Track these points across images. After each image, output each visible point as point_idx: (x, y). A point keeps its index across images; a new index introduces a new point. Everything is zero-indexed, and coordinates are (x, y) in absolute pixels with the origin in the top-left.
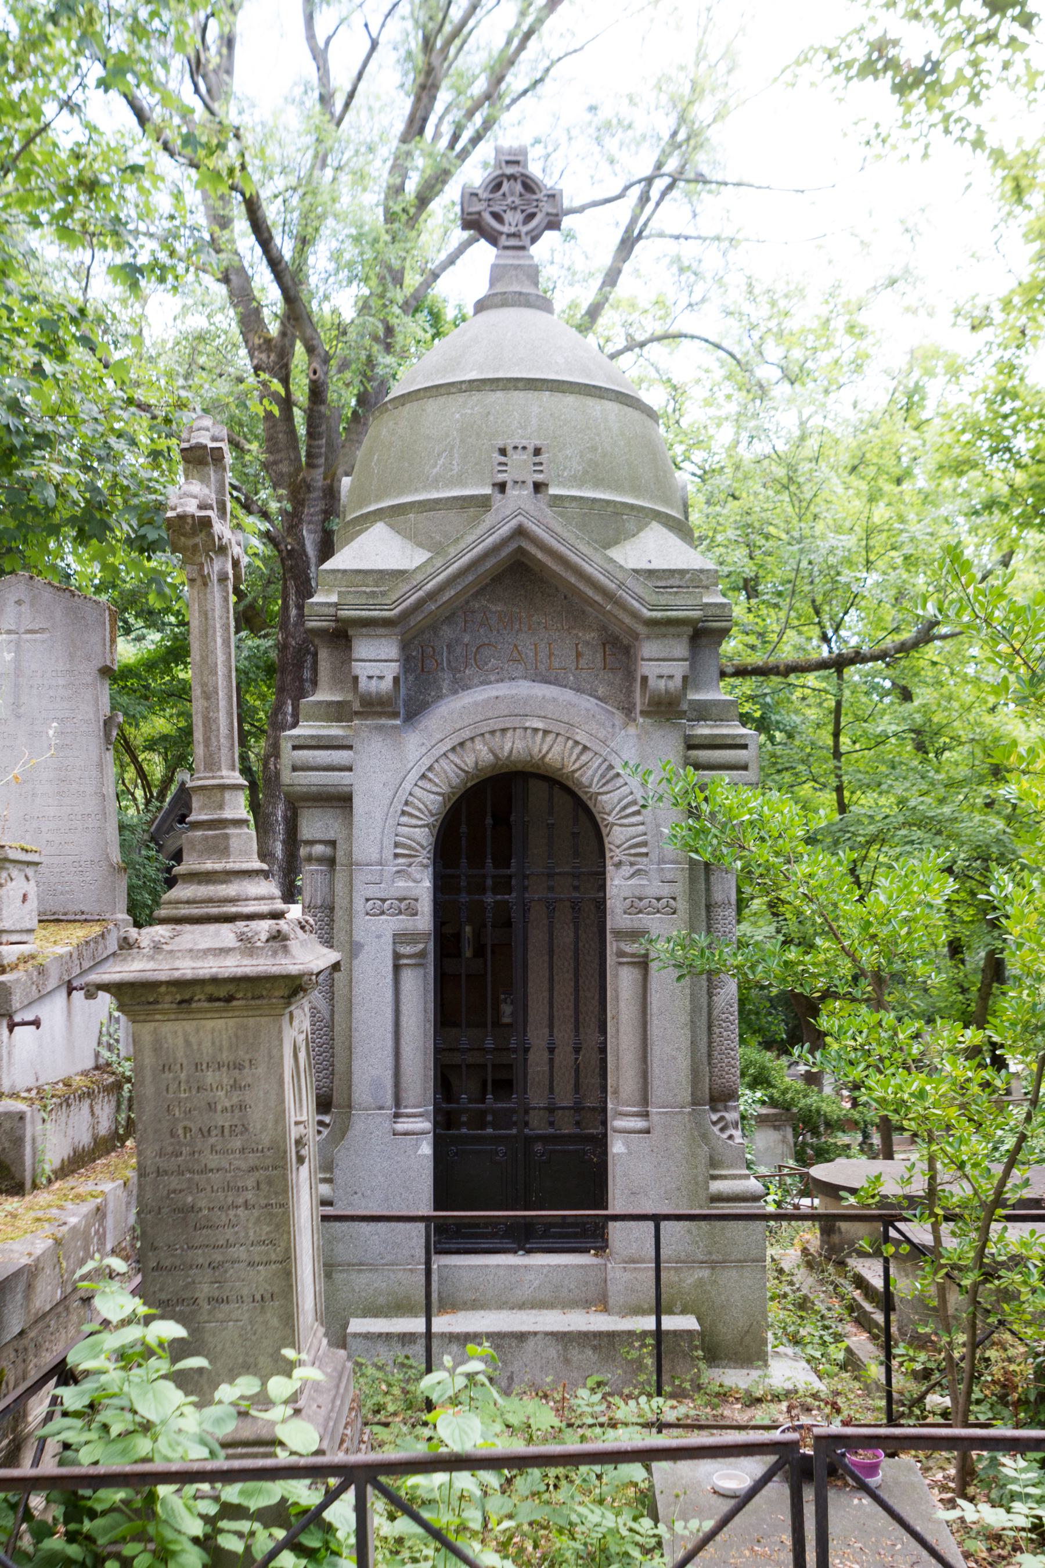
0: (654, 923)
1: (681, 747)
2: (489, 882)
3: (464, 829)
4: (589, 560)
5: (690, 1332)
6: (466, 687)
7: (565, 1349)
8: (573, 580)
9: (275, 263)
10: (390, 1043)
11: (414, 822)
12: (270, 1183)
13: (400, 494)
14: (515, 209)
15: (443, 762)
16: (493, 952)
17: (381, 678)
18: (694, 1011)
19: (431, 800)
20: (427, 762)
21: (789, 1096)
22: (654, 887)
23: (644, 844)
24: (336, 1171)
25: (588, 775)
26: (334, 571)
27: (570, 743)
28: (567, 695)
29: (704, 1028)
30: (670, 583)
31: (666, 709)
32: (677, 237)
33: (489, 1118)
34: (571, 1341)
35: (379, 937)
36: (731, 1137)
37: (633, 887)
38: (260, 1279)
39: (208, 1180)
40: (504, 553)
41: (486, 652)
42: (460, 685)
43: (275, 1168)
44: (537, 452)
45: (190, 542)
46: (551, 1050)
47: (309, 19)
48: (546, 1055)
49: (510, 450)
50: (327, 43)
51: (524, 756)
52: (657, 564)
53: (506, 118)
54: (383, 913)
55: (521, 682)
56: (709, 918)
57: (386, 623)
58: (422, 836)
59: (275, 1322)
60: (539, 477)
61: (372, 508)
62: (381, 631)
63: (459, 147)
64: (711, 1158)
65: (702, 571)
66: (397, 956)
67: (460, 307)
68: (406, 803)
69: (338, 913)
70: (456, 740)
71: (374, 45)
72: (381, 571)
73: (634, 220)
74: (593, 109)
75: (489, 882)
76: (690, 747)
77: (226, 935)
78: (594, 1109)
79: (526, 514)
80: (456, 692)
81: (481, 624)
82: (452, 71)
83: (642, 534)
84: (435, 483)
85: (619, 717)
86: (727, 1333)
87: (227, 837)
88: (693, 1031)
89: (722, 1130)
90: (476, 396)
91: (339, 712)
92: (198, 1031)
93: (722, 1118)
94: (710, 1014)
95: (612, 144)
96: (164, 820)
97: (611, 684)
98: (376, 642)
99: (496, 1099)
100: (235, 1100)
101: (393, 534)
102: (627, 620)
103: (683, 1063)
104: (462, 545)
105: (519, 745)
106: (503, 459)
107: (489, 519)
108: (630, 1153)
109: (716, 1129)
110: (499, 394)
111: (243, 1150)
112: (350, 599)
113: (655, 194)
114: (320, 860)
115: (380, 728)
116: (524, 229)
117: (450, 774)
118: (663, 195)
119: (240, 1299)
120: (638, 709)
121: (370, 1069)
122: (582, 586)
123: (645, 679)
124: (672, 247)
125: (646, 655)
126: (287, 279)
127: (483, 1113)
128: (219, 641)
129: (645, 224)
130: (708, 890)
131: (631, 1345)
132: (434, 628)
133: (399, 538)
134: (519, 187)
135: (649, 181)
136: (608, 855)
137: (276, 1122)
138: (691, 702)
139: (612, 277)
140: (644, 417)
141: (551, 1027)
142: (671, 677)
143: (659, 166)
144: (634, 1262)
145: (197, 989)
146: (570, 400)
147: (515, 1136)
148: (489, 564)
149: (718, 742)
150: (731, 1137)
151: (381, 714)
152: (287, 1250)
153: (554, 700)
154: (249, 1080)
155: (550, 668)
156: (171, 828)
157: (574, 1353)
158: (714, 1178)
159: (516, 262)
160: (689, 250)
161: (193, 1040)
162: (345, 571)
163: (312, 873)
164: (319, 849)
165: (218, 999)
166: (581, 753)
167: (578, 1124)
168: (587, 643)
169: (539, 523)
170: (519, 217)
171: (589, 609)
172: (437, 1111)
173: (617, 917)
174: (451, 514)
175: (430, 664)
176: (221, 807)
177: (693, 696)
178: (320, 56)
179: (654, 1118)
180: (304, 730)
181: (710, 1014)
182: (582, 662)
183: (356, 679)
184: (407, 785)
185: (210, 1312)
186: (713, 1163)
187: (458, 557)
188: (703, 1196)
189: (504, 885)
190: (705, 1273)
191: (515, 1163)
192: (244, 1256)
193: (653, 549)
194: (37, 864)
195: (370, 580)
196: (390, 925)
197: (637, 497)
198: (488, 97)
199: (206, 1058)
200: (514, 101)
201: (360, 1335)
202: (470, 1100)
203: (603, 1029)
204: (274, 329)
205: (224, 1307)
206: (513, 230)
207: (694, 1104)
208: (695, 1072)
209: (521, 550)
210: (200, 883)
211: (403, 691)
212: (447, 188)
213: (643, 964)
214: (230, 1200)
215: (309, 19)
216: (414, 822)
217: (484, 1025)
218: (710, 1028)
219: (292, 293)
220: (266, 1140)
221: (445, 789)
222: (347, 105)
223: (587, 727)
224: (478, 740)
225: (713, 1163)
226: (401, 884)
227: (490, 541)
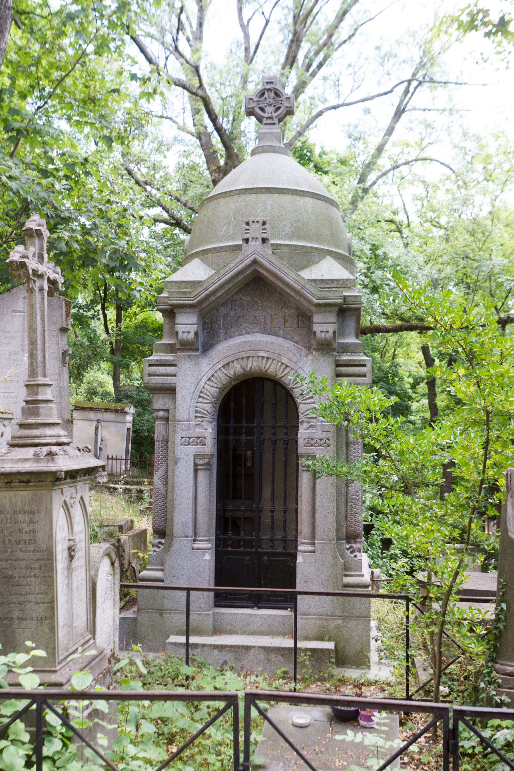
0: (319, 452)
1: (333, 366)
3: (232, 404)
5: (329, 650)
6: (232, 337)
7: (268, 655)
9: (219, 129)
11: (205, 401)
12: (46, 566)
13: (207, 244)
14: (271, 105)
15: (219, 373)
17: (189, 332)
18: (338, 494)
19: (212, 390)
20: (211, 372)
21: (478, 540)
22: (318, 434)
24: (166, 566)
25: (289, 379)
26: (171, 282)
27: (280, 364)
28: (279, 340)
29: (343, 503)
30: (332, 285)
31: (325, 347)
32: (424, 110)
33: (242, 543)
35: (187, 455)
36: (355, 556)
37: (312, 433)
38: (40, 610)
39: (19, 564)
42: (229, 336)
43: (48, 560)
44: (264, 223)
45: (17, 273)
46: (272, 512)
47: (240, 10)
48: (270, 514)
49: (251, 222)
50: (248, 22)
51: (257, 370)
52: (325, 277)
53: (335, 55)
54: (189, 444)
55: (258, 334)
56: (347, 449)
57: (191, 306)
59: (47, 630)
60: (264, 236)
62: (189, 310)
63: (311, 70)
65: (347, 280)
66: (196, 465)
67: (322, 148)
68: (201, 392)
69: (170, 444)
71: (267, 22)
72: (193, 282)
73: (401, 102)
74: (378, 48)
75: (244, 430)
76: (338, 366)
77: (30, 452)
80: (226, 339)
82: (308, 33)
84: (221, 240)
85: (304, 351)
86: (351, 650)
87: (38, 408)
88: (337, 505)
90: (243, 197)
91: (171, 349)
92: (15, 496)
93: (351, 547)
94: (347, 496)
95: (388, 65)
97: (301, 335)
98: (187, 316)
100: (31, 528)
102: (306, 304)
103: (331, 520)
104: (227, 269)
105: (255, 365)
106: (247, 227)
107: (241, 256)
108: (305, 562)
109: (348, 552)
110: (253, 195)
111: (34, 551)
112: (174, 295)
113: (411, 89)
114: (162, 419)
115: (189, 356)
116: (275, 115)
117: (222, 378)
118: (416, 88)
119: (32, 619)
121: (182, 518)
122: (285, 288)
124: (420, 115)
127: (239, 541)
128: (39, 318)
129: (406, 104)
132: (217, 309)
134: (272, 95)
135: (409, 82)
137: (49, 539)
139: (390, 131)
140: (328, 205)
142: (327, 332)
143: (414, 75)
144: (306, 615)
145: (13, 477)
146: (288, 197)
148: (240, 278)
149: (352, 363)
150: (355, 556)
151: (190, 350)
152: (53, 597)
153: (272, 343)
154: (37, 519)
155: (271, 327)
157: (273, 657)
158: (346, 576)
159: (270, 131)
160: (429, 116)
161: (13, 500)
162: (176, 282)
163: (158, 425)
164: (161, 414)
165: (23, 482)
166: (285, 369)
167: (284, 547)
168: (290, 315)
169: (264, 258)
170: (273, 109)
172: (217, 539)
173: (302, 449)
174: (228, 254)
176: (37, 394)
178: (244, 28)
179: (317, 545)
181: (347, 496)
182: (287, 324)
183: (177, 333)
184: (202, 384)
185: (18, 624)
187: (225, 274)
188: (340, 584)
189: (250, 432)
190: (340, 622)
191: (253, 564)
192: (33, 599)
193: (329, 269)
194: (11, 419)
195: (188, 286)
196: (192, 450)
197: (320, 244)
198: (325, 45)
199: (19, 509)
200: (340, 45)
201: (172, 643)
203: (297, 503)
204: (222, 162)
205: (25, 622)
206: (269, 115)
208: (338, 524)
209: (255, 270)
210: (25, 429)
212: (306, 90)
214: (28, 574)
215: (240, 10)
216: (205, 401)
218: (347, 502)
219: (228, 144)
220: (44, 546)
221: (219, 385)
222: (255, 52)
223: (288, 356)
224: (235, 362)
226: (198, 430)
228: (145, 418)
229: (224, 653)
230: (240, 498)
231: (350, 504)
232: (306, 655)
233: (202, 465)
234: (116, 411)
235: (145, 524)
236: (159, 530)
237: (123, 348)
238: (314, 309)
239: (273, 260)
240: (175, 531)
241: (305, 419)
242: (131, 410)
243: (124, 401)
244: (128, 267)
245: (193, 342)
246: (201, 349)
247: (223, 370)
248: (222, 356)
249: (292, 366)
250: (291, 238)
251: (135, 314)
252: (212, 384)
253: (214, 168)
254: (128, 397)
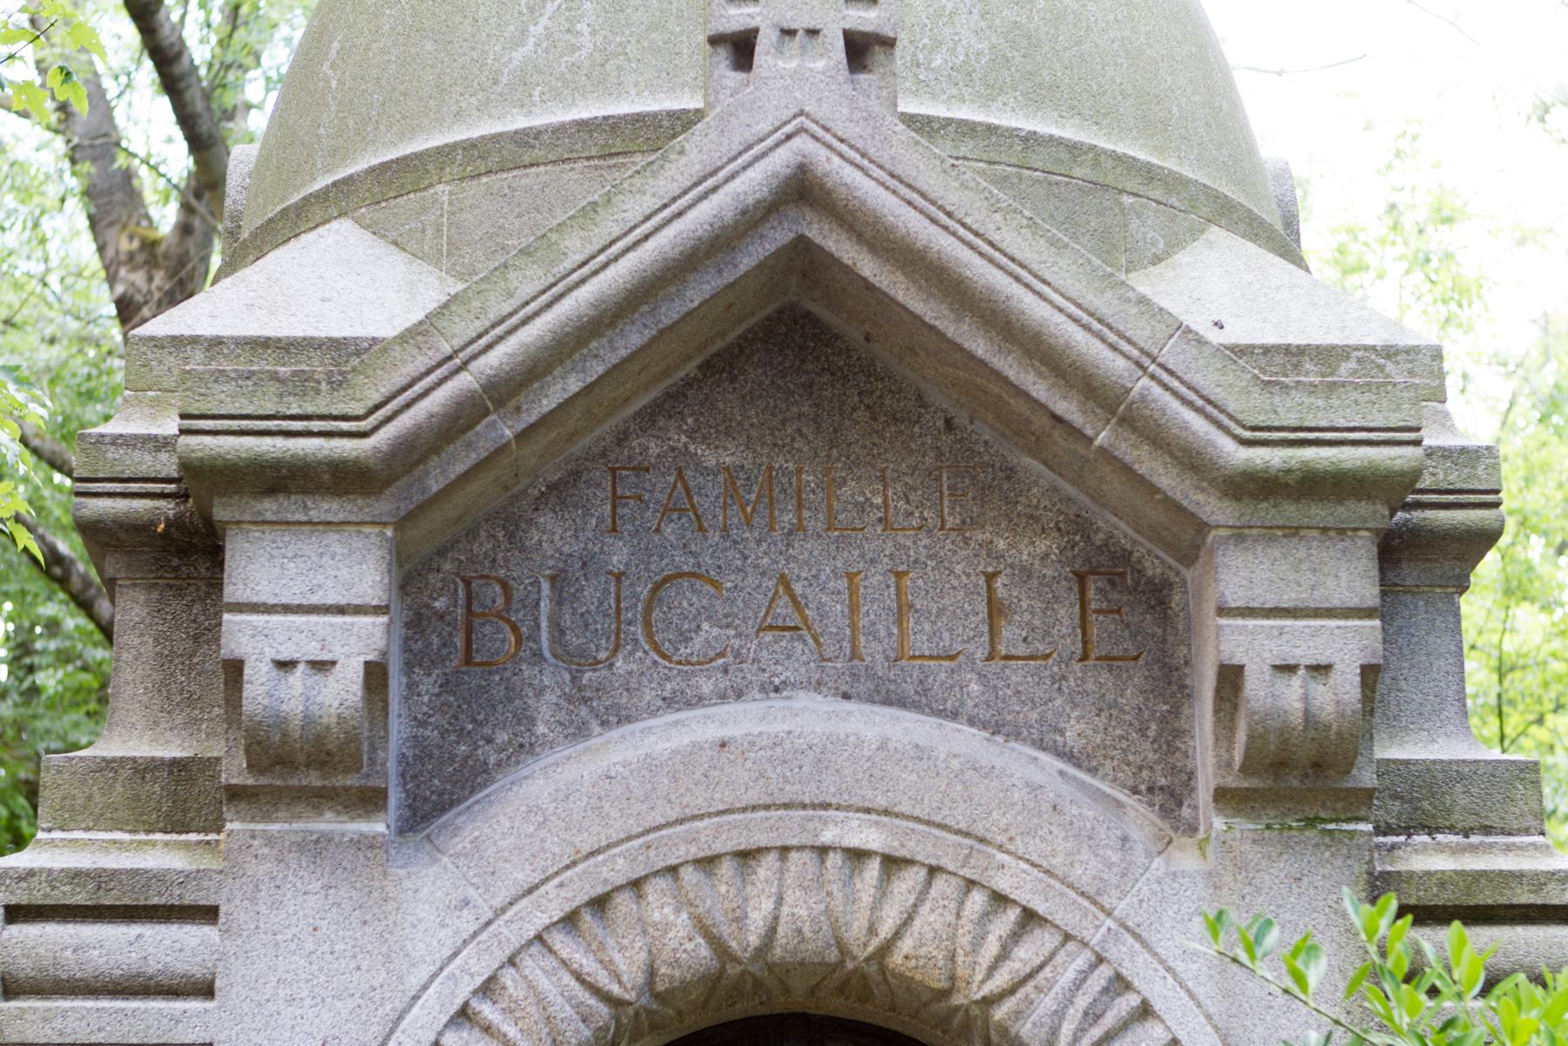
4: (1034, 280)
8: (980, 346)
15: (534, 965)
17: (321, 666)
20: (477, 965)
27: (978, 899)
28: (965, 740)
31: (1306, 782)
40: (749, 258)
41: (686, 599)
42: (596, 710)
51: (817, 946)
57: (345, 479)
60: (866, 19)
70: (579, 889)
79: (822, 132)
80: (579, 732)
81: (669, 510)
83: (1181, 258)
84: (521, 89)
85: (1140, 818)
91: (177, 797)
98: (309, 546)
101: (381, 248)
102: (1167, 478)
104: (608, 226)
105: (801, 908)
112: (224, 399)
115: (317, 847)
120: (1206, 783)
122: (1010, 366)
123: (1231, 677)
125: (1235, 599)
126: (194, 96)
132: (510, 522)
133: (398, 257)
138: (1388, 768)
142: (1321, 670)
148: (698, 291)
149: (1486, 897)
151: (319, 799)
155: (900, 655)
166: (1016, 936)
168: (1026, 573)
169: (864, 160)
175: (496, 639)
180: (54, 854)
182: (1011, 635)
183: (234, 670)
187: (591, 265)
204: (165, 217)
209: (802, 246)
211: (398, 728)
219: (204, 127)
223: (1033, 848)
224: (656, 890)
227: (701, 217)
238: (1216, 510)
239: (931, 181)
245: (352, 738)
248: (556, 848)
249: (1066, 917)
250: (990, 93)
253: (126, 245)
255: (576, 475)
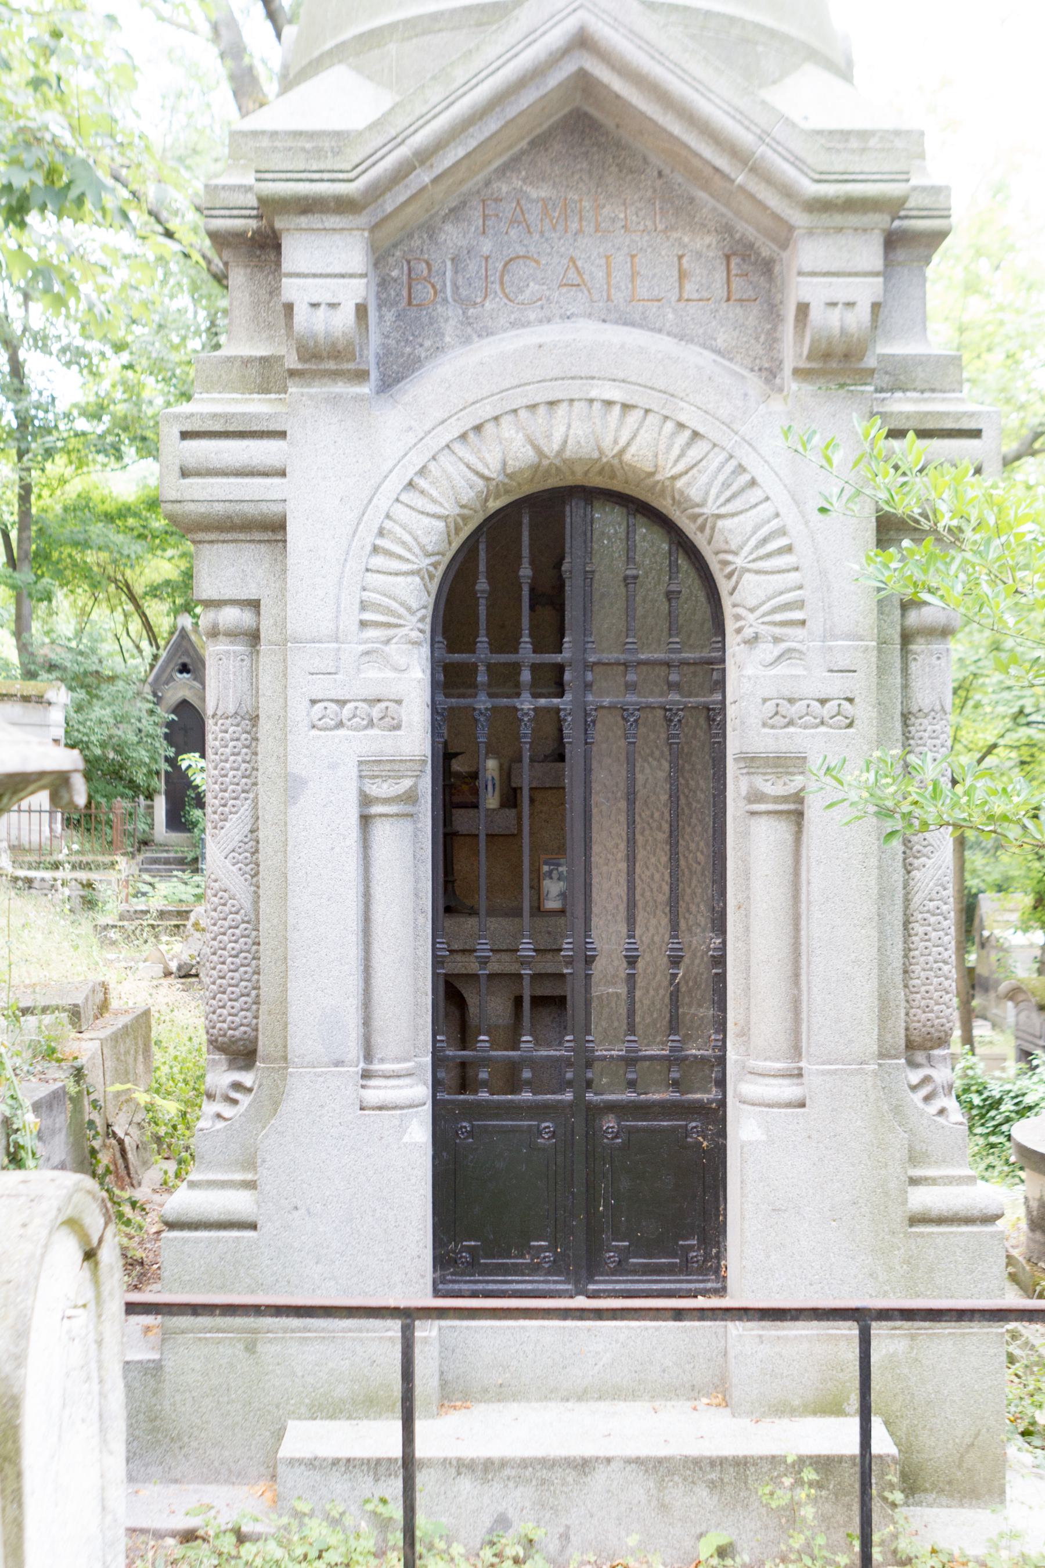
0: (816, 744)
2: (526, 676)
3: (482, 585)
6: (486, 332)
7: (661, 1486)
10: (353, 952)
11: (395, 565)
15: (445, 459)
16: (532, 801)
22: (813, 679)
23: (800, 605)
27: (669, 426)
28: (665, 344)
31: (839, 364)
33: (527, 1074)
34: (671, 1473)
35: (333, 766)
37: (782, 679)
41: (521, 270)
42: (475, 329)
46: (632, 961)
51: (588, 451)
54: (340, 725)
55: (582, 323)
57: (344, 206)
58: (412, 596)
61: (330, 44)
62: (333, 221)
64: (911, 1149)
66: (366, 800)
68: (381, 533)
69: (265, 726)
75: (526, 676)
78: (704, 1059)
80: (467, 340)
81: (512, 222)
85: (755, 383)
89: (927, 1099)
94: (907, 901)
96: (163, 669)
99: (538, 1042)
102: (774, 201)
103: (864, 990)
109: (918, 1097)
114: (233, 634)
115: (335, 400)
125: (807, 266)
130: (905, 687)
131: (776, 1481)
132: (430, 229)
136: (730, 626)
138: (882, 358)
141: (631, 921)
147: (571, 1105)
148: (527, 98)
150: (942, 1112)
151: (335, 375)
155: (632, 299)
156: (171, 679)
157: (676, 1494)
158: (914, 1181)
164: (230, 616)
166: (688, 445)
168: (699, 255)
171: (702, 195)
172: (438, 1061)
175: (423, 292)
177: (884, 348)
181: (907, 901)
182: (690, 288)
183: (289, 308)
184: (383, 502)
186: (914, 1158)
196: (355, 745)
201: (300, 1461)
202: (494, 1045)
203: (719, 925)
207: (882, 1055)
209: (584, 81)
211: (374, 339)
213: (795, 813)
216: (395, 565)
217: (517, 913)
218: (906, 924)
221: (450, 509)
224: (506, 421)
225: (914, 1158)
228: (93, 716)
229: (497, 1487)
230: (473, 912)
231: (918, 928)
232: (799, 1482)
233: (386, 801)
234: (26, 699)
235: (183, 1022)
236: (233, 1041)
237: (37, 554)
238: (799, 218)
240: (293, 1043)
241: (763, 630)
242: (60, 696)
243: (44, 675)
244: (73, 193)
245: (350, 343)
246: (374, 375)
247: (457, 447)
251: (63, 481)
252: (420, 502)
254: (52, 667)
255: (464, 203)
